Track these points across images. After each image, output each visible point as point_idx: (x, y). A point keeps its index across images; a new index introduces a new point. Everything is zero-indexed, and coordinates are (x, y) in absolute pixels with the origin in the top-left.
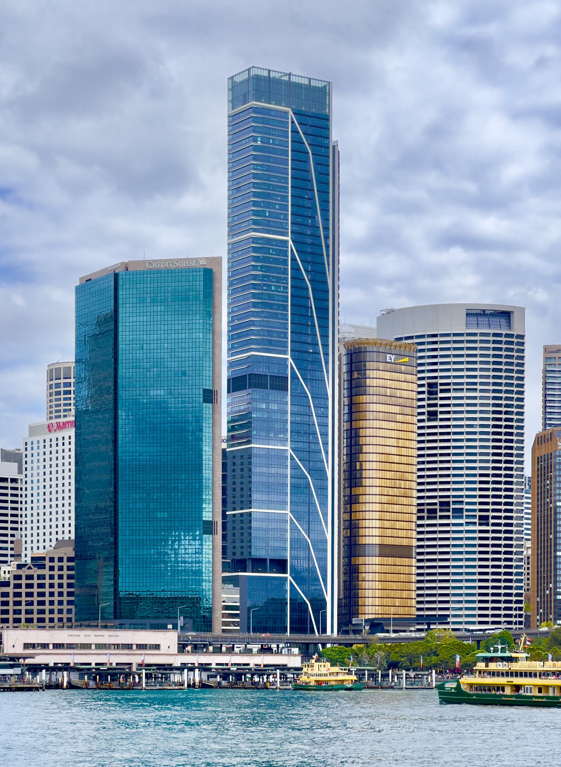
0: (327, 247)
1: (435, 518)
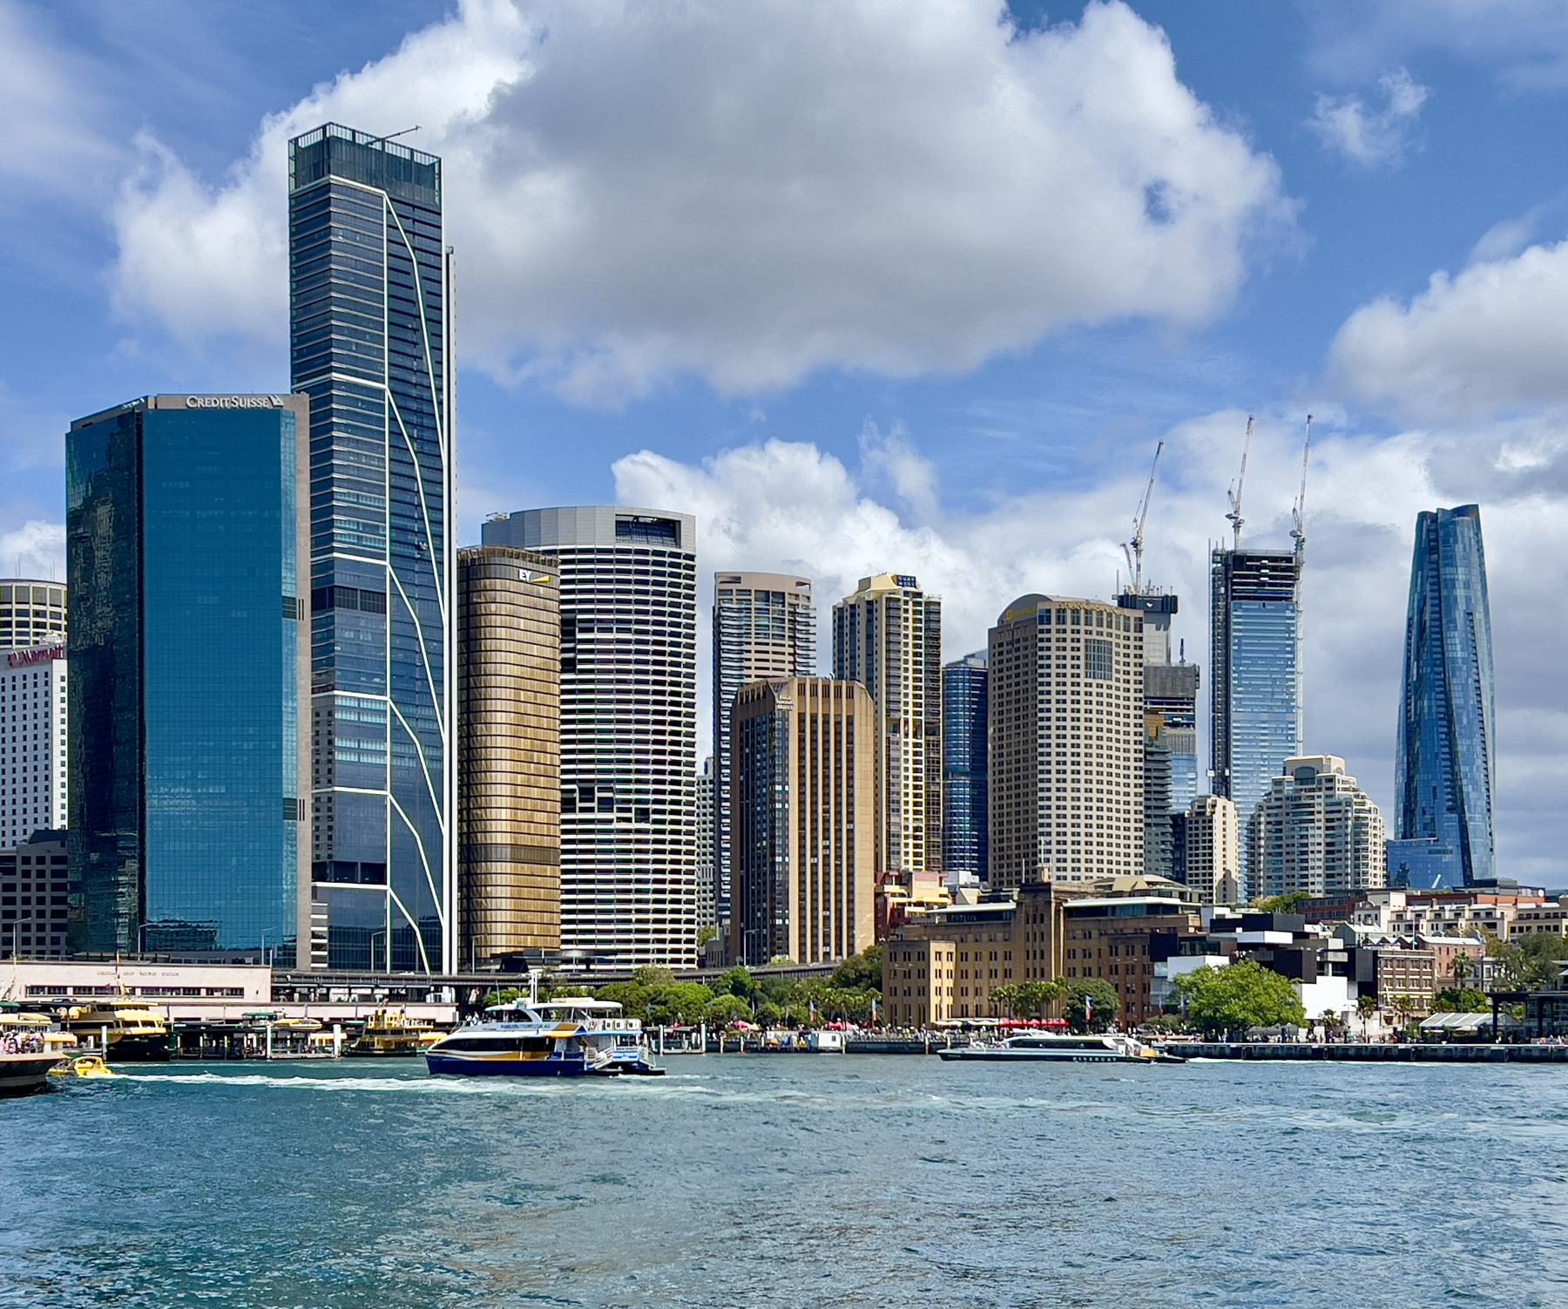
0: (440, 403)
1: (573, 811)
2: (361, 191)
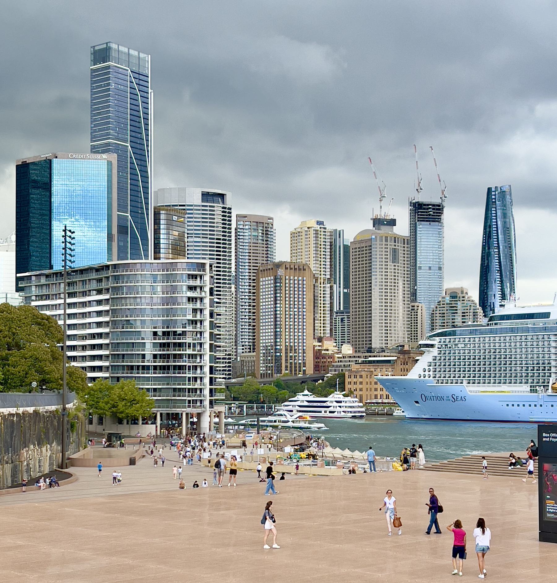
0: (148, 151)
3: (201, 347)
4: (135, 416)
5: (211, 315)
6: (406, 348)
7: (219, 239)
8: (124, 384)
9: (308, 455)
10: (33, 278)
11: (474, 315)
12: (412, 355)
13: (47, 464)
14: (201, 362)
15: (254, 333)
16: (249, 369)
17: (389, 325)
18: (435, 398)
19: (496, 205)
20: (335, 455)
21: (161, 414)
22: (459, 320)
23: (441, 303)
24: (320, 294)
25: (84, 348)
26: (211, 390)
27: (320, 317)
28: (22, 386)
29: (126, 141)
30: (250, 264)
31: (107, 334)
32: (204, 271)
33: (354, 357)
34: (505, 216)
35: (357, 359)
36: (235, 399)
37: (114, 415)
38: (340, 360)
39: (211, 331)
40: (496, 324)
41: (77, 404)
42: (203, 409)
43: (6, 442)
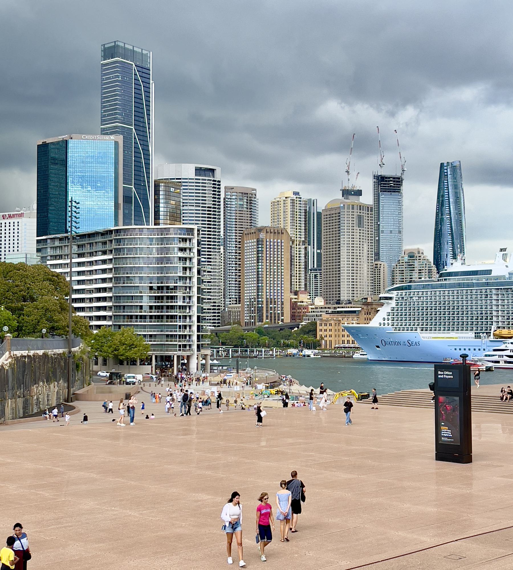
0: (149, 133)
2: (127, 63)
3: (190, 299)
4: (133, 358)
5: (199, 272)
6: (369, 300)
7: (210, 207)
8: (124, 331)
9: (277, 391)
10: (49, 241)
11: (429, 272)
12: (374, 306)
13: (55, 398)
14: (189, 312)
15: (239, 287)
16: (235, 319)
17: (355, 280)
18: (393, 343)
19: (449, 179)
20: (301, 392)
21: (156, 357)
22: (415, 276)
23: (401, 262)
24: (296, 254)
25: (91, 300)
26: (198, 336)
27: (296, 274)
28: (35, 333)
29: (131, 125)
30: (236, 229)
31: (111, 289)
32: (193, 235)
33: (325, 308)
34: (456, 187)
35: (328, 310)
36: (223, 344)
37: (116, 357)
38: (313, 310)
39: (199, 286)
40: (445, 280)
41: (82, 348)
42: (192, 352)
43: (18, 379)
